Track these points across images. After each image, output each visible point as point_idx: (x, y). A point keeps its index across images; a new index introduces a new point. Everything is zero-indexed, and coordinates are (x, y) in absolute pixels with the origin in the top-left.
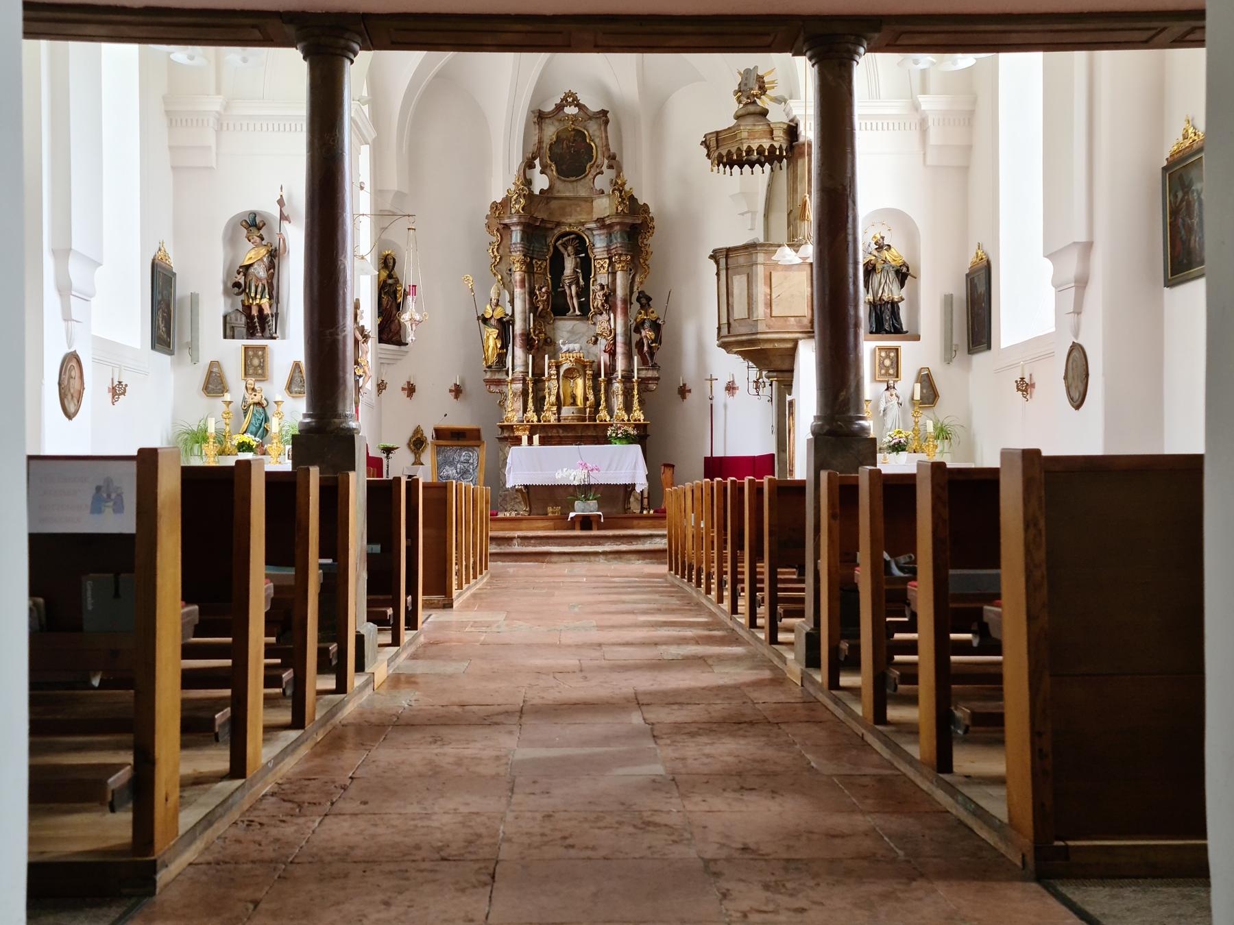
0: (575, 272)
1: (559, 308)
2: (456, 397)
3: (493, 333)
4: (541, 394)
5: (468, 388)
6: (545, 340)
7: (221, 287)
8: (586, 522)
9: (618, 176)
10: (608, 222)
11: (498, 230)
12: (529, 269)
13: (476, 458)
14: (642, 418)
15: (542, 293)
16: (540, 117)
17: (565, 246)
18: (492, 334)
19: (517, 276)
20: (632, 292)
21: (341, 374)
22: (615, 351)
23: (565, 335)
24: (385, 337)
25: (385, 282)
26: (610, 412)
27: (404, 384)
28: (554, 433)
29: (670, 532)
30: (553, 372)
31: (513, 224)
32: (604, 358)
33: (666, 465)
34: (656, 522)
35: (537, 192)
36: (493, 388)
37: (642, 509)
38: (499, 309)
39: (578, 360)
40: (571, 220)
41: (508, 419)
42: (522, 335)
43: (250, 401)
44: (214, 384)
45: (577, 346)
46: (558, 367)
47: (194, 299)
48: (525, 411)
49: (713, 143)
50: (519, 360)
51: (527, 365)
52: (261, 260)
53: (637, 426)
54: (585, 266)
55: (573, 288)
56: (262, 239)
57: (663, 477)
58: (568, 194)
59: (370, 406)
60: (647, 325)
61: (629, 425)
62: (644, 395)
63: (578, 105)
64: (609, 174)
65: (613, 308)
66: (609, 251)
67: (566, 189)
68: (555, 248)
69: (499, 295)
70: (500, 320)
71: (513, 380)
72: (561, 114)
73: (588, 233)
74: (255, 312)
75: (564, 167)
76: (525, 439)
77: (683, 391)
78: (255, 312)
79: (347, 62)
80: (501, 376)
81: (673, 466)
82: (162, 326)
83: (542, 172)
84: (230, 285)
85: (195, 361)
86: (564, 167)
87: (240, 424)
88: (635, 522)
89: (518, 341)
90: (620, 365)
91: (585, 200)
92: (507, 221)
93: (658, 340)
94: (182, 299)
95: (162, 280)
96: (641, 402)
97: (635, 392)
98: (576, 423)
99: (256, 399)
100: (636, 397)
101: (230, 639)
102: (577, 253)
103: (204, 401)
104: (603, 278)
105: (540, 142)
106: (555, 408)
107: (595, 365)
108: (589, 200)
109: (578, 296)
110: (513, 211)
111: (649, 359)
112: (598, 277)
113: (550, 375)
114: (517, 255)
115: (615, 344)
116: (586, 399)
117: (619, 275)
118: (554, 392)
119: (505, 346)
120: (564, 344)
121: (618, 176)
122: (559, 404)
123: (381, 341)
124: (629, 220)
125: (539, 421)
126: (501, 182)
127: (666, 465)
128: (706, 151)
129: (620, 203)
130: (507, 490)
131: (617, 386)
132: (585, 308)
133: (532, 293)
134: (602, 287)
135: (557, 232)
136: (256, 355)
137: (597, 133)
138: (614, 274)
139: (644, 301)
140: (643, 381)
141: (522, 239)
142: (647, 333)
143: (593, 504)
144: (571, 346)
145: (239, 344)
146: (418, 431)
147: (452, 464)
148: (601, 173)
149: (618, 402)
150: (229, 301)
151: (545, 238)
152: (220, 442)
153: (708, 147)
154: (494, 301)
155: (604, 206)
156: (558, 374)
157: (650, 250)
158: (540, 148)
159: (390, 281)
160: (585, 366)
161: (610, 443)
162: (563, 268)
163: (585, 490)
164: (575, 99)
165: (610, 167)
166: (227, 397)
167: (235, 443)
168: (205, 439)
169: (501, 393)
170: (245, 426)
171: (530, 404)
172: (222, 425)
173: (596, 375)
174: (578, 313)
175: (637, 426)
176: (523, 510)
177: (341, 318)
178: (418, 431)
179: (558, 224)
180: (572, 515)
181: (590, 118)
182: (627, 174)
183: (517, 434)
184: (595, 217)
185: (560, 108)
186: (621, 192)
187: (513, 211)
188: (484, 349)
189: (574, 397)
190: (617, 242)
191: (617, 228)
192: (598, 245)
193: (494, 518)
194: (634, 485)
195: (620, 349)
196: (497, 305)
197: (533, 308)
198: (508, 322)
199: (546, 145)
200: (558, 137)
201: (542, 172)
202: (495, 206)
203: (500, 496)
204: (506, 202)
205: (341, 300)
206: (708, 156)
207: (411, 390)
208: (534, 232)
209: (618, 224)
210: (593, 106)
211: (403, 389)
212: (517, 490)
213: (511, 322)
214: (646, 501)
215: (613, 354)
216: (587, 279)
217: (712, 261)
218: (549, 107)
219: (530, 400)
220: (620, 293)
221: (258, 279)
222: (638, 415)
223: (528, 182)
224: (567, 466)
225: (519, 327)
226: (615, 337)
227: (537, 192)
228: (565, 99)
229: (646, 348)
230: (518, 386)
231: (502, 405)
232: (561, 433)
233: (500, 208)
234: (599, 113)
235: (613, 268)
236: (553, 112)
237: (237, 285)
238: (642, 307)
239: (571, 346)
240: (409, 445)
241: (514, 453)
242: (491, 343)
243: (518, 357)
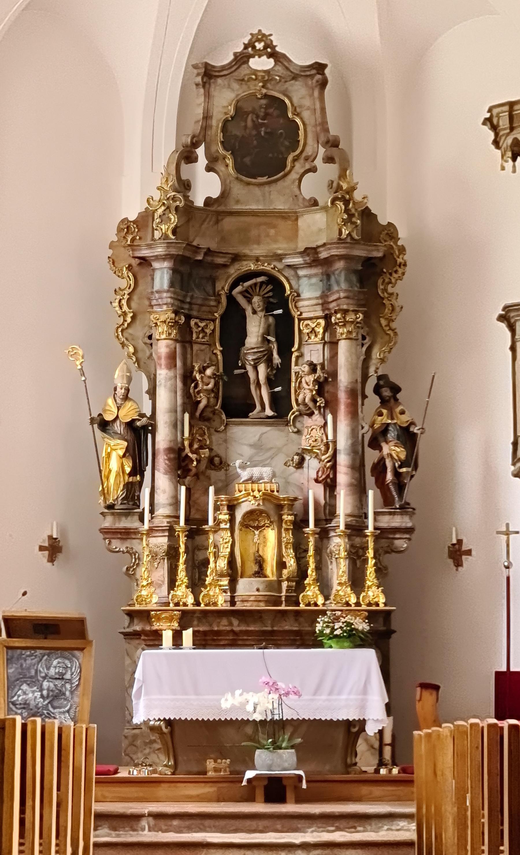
0: (265, 340)
1: (238, 407)
2: (52, 559)
3: (119, 446)
4: (200, 556)
5: (72, 542)
6: (211, 460)
8: (275, 789)
9: (343, 175)
10: (324, 255)
11: (130, 268)
12: (184, 336)
13: (79, 670)
14: (382, 600)
15: (206, 379)
16: (209, 75)
17: (248, 295)
18: (115, 453)
19: (163, 347)
20: (365, 377)
22: (334, 480)
23: (247, 451)
26: (325, 589)
28: (223, 625)
29: (419, 808)
30: (224, 516)
31: (157, 258)
32: (316, 493)
33: (425, 686)
34: (401, 790)
35: (199, 202)
36: (116, 544)
37: (381, 763)
38: (129, 405)
39: (268, 497)
40: (258, 251)
41: (141, 600)
42: (169, 450)
45: (266, 471)
46: (232, 508)
48: (172, 584)
49: (504, 123)
50: (163, 497)
51: (176, 504)
53: (372, 616)
54: (283, 331)
55: (262, 369)
57: (418, 706)
58: (254, 207)
60: (392, 435)
61: (355, 613)
62: (388, 559)
63: (274, 55)
64: (327, 172)
65: (331, 405)
66: (324, 304)
67: (251, 198)
68: (231, 298)
69: (129, 380)
70: (130, 425)
71: (151, 530)
72: (243, 71)
73: (289, 273)
75: (247, 160)
76: (167, 636)
77: (457, 553)
80: (131, 523)
81: (436, 688)
83: (209, 169)
86: (247, 160)
88: (365, 790)
89: (162, 461)
90: (344, 504)
91: (283, 216)
92: (145, 253)
93: (411, 460)
96: (380, 571)
97: (370, 553)
98: (262, 607)
100: (371, 562)
101: (280, 388)
102: (268, 308)
104: (314, 352)
105: (207, 117)
106: (225, 582)
107: (298, 504)
108: (291, 217)
109: (271, 382)
110: (157, 235)
111: (395, 491)
112: (306, 350)
113: (217, 522)
114: (163, 313)
115: (334, 468)
116: (281, 565)
117: (343, 346)
118: (225, 551)
119: (138, 469)
120: (243, 467)
121: (343, 175)
122: (233, 573)
124: (360, 252)
125: (198, 604)
126: (137, 185)
127: (425, 686)
128: (491, 135)
129: (345, 222)
130: (137, 727)
131: (338, 544)
132: (281, 405)
133: (188, 378)
134: (313, 368)
135: (234, 271)
137: (307, 102)
138: (334, 344)
139: (386, 393)
140: (383, 534)
141: (172, 284)
142: (393, 450)
143: (288, 756)
144: (256, 471)
147: (34, 681)
148: (314, 170)
149: (339, 570)
151: (213, 281)
153: (494, 128)
154: (120, 392)
155: (318, 228)
156: (232, 520)
157: (397, 304)
158: (206, 128)
160: (279, 507)
161: (321, 645)
162: (244, 335)
163: (274, 730)
164: (269, 45)
165: (329, 160)
169: (131, 552)
171: (182, 574)
173: (300, 523)
174: (269, 412)
175: (372, 616)
176: (162, 766)
179: (236, 258)
180: (250, 774)
181: (295, 77)
182: (359, 173)
183: (156, 626)
184: (301, 246)
185: (241, 59)
186: (346, 203)
187: (157, 235)
188: (102, 475)
189: (260, 562)
190: (341, 288)
191: (340, 265)
192: (306, 293)
193: (106, 778)
194: (362, 723)
195: (343, 478)
196: (126, 398)
197: (190, 404)
198: (144, 427)
199: (216, 122)
200: (237, 109)
201: (209, 169)
202: (125, 227)
203: (117, 737)
204: (145, 220)
206: (496, 143)
208: (192, 270)
209: (341, 257)
210: (301, 57)
211: (42, 548)
212: (153, 729)
213: (150, 428)
214: (387, 751)
215: (330, 485)
216: (285, 351)
217: (503, 326)
218: (226, 58)
219: (182, 567)
220: (344, 378)
222: (375, 595)
223: (185, 186)
224: (243, 686)
225: (163, 437)
226: (334, 456)
227: (199, 202)
228: (251, 45)
229: (389, 476)
230: (161, 541)
231: (131, 573)
232: (237, 626)
233: (132, 230)
234: (311, 67)
235: (333, 334)
236: (230, 66)
238: (384, 402)
239: (256, 471)
241: (149, 663)
242: (114, 465)
243: (162, 488)
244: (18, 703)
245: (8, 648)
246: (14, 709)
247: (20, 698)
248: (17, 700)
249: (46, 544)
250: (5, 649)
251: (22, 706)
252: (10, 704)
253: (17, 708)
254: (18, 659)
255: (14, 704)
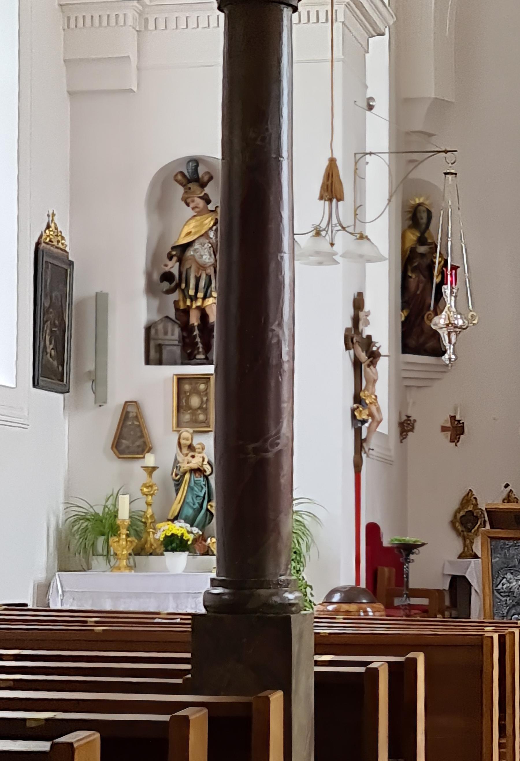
7: (141, 282)
21: (271, 515)
24: (412, 342)
25: (413, 250)
27: (444, 420)
43: (185, 466)
44: (130, 438)
47: (101, 301)
52: (206, 235)
56: (208, 201)
59: (387, 462)
74: (194, 319)
78: (194, 319)
79: (286, 12)
82: (50, 348)
84: (156, 277)
85: (101, 401)
87: (170, 504)
94: (82, 302)
95: (51, 273)
99: (195, 463)
103: (114, 467)
123: (406, 349)
136: (196, 391)
145: (169, 372)
146: (469, 498)
150: (156, 303)
152: (138, 535)
159: (422, 249)
166: (150, 460)
167: (160, 536)
168: (114, 530)
170: (176, 508)
172: (140, 505)
177: (272, 423)
178: (469, 498)
205: (272, 396)
207: (456, 430)
211: (444, 429)
221: (202, 267)
237: (167, 277)
240: (453, 523)
244: (502, 591)
245: (492, 538)
246: (499, 596)
247: (504, 586)
248: (503, 588)
249: (449, 425)
250: (489, 540)
251: (507, 594)
252: (495, 591)
253: (501, 596)
254: (502, 548)
255: (498, 591)
